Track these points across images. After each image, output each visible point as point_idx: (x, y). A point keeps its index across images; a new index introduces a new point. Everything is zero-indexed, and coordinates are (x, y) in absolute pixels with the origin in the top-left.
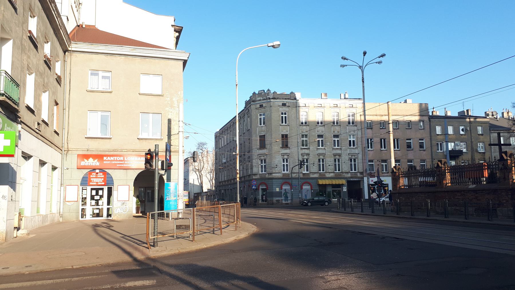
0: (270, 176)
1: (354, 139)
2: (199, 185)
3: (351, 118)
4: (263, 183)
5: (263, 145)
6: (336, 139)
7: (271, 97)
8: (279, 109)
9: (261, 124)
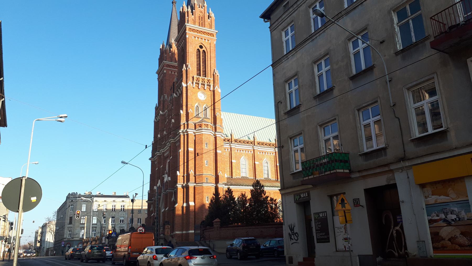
0: (73, 240)
1: (123, 219)
2: (53, 242)
3: (123, 208)
4: (69, 243)
5: (71, 223)
6: (113, 219)
7: (78, 197)
8: (81, 203)
9: (71, 211)
